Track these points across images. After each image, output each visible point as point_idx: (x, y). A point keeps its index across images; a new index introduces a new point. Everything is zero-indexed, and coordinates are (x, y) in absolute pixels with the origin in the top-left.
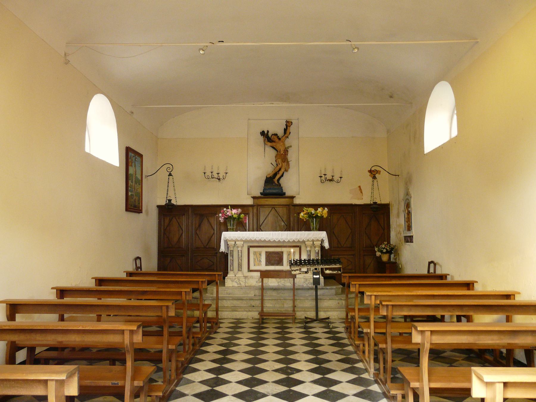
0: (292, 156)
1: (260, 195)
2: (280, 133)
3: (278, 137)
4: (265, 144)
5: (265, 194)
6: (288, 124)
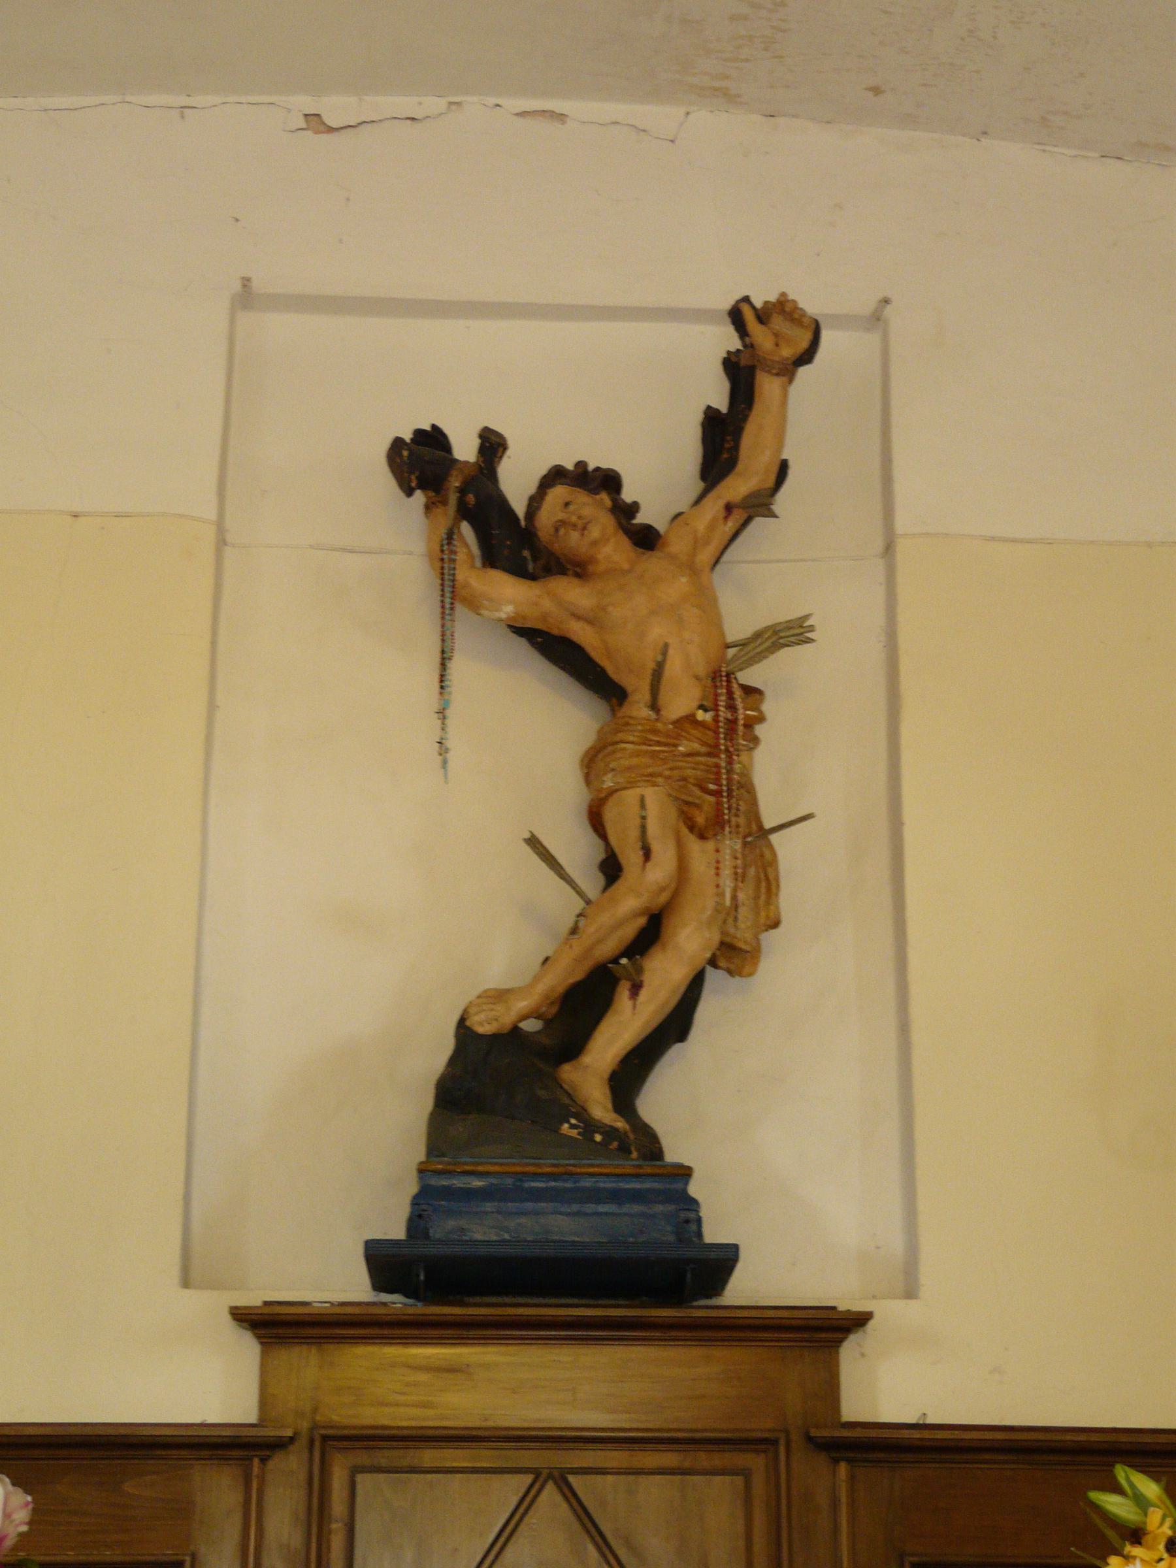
0: (800, 763)
1: (352, 1285)
2: (658, 470)
3: (625, 512)
4: (451, 595)
5: (435, 1279)
6: (764, 349)
